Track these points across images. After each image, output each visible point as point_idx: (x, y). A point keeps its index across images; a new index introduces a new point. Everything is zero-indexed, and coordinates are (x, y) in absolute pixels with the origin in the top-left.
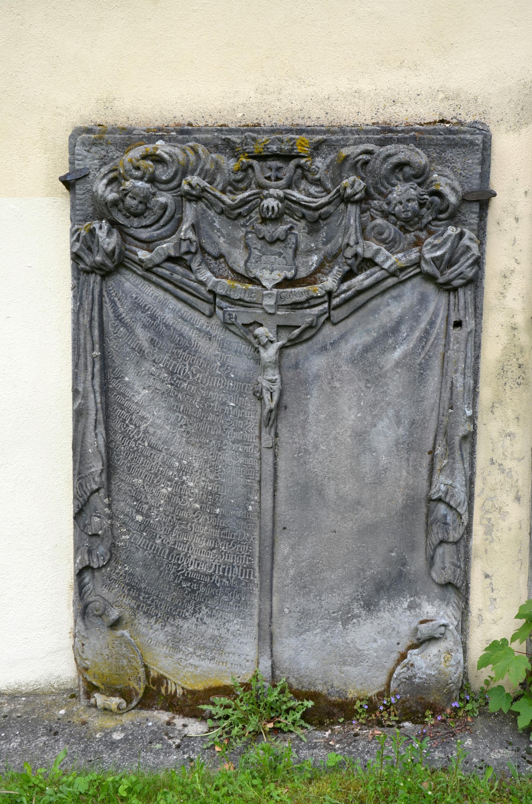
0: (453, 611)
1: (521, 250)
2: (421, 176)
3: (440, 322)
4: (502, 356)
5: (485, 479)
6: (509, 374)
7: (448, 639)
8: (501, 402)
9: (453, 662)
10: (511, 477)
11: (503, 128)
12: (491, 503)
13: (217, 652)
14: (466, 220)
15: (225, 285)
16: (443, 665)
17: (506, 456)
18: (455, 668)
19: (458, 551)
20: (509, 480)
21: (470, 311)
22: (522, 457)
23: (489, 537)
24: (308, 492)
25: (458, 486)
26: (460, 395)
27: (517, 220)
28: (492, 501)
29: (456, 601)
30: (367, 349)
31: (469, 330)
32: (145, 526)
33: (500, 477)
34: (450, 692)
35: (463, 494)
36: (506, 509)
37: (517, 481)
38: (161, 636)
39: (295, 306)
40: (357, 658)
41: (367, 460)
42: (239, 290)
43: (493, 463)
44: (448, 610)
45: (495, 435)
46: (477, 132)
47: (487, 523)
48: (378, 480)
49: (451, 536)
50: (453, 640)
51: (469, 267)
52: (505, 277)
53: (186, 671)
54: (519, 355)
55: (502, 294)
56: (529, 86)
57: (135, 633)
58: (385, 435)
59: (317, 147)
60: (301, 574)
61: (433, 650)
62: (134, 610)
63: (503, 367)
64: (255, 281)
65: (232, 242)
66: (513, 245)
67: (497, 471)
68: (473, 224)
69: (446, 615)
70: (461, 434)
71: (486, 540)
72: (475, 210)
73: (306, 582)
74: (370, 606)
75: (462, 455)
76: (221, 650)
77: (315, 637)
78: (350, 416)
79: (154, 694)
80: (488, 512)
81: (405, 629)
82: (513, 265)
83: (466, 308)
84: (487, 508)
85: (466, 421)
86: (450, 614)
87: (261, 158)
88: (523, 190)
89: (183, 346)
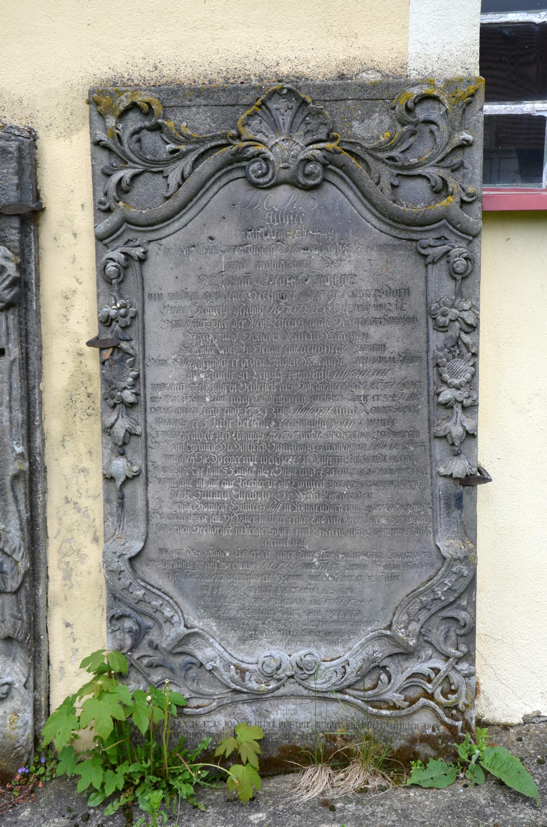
0: (20, 667)
1: (82, 269)
4: (70, 384)
5: (60, 519)
6: (78, 405)
7: (15, 698)
8: (71, 435)
9: (20, 724)
10: (88, 517)
11: (53, 134)
12: (68, 545)
14: (6, 237)
16: (8, 728)
17: (81, 494)
18: (22, 730)
19: (18, 602)
20: (85, 519)
21: (13, 337)
22: (97, 494)
23: (68, 582)
25: (13, 530)
26: (7, 431)
27: (75, 235)
28: (70, 543)
29: (23, 656)
31: (12, 358)
33: (76, 517)
34: (19, 757)
35: (18, 539)
36: (85, 551)
37: (94, 520)
43: (68, 502)
44: (15, 667)
45: (68, 471)
46: (13, 138)
47: (65, 567)
49: (9, 586)
50: (20, 699)
51: (5, 288)
52: (67, 298)
54: (87, 384)
55: (65, 316)
56: (76, 89)
63: (71, 396)
66: (73, 263)
67: (73, 510)
68: (13, 241)
69: (13, 672)
70: (11, 474)
71: (65, 585)
72: (14, 225)
75: (15, 498)
80: (65, 555)
82: (74, 285)
83: (8, 334)
84: (64, 551)
85: (16, 459)
86: (17, 670)
88: (79, 203)
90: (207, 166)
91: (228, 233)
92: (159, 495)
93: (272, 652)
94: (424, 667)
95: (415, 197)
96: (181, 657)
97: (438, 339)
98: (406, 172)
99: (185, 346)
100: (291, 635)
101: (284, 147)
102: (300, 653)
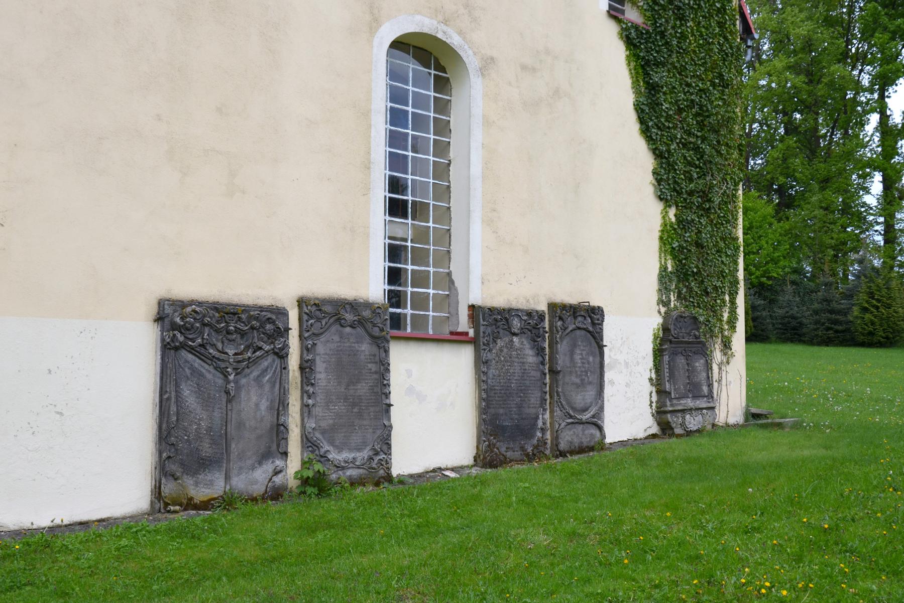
2: (273, 322)
3: (279, 368)
13: (210, 486)
15: (217, 355)
24: (240, 425)
30: (258, 376)
32: (188, 440)
38: (191, 482)
39: (239, 362)
40: (256, 482)
41: (258, 413)
42: (223, 356)
48: (262, 420)
53: (200, 494)
57: (184, 482)
58: (264, 405)
59: (243, 311)
60: (239, 454)
61: (280, 476)
62: (183, 473)
64: (226, 353)
65: (217, 340)
73: (241, 457)
74: (260, 463)
76: (212, 485)
77: (243, 476)
78: (254, 399)
79: (190, 505)
81: (271, 470)
87: (227, 313)
89: (201, 375)
90: (332, 320)
91: (336, 338)
92: (317, 411)
93: (346, 455)
94: (381, 457)
95: (376, 332)
96: (323, 458)
97: (382, 368)
98: (375, 325)
99: (326, 368)
100: (351, 450)
101: (349, 317)
102: (353, 455)
